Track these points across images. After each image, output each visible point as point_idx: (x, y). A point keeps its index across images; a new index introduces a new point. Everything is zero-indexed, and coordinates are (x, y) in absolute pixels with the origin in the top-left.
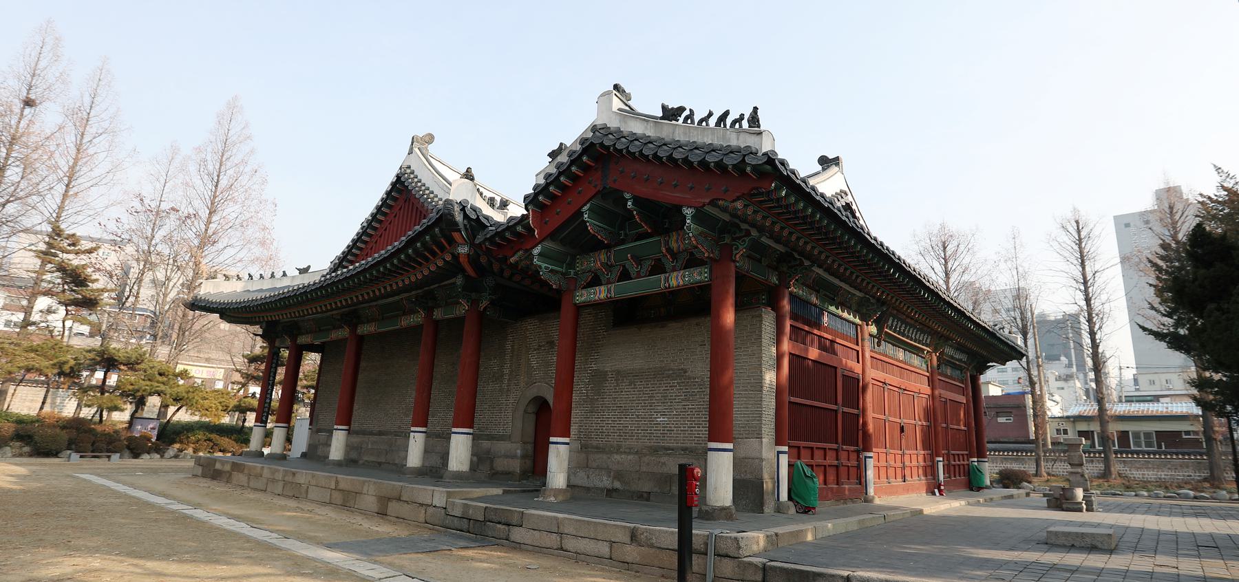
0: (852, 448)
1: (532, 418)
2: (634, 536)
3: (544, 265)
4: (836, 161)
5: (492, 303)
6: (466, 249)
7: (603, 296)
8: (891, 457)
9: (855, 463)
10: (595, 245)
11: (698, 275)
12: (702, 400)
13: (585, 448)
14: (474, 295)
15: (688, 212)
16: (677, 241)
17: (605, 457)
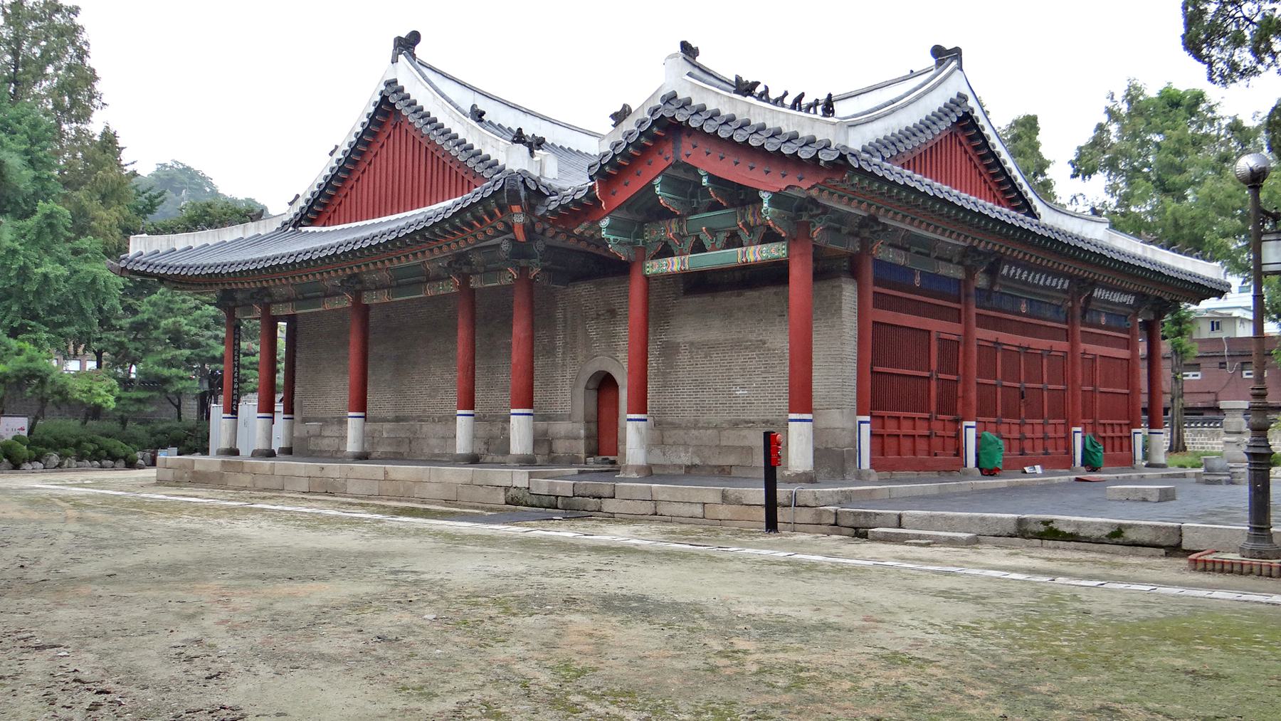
0: (951, 417)
1: (594, 394)
2: (725, 498)
3: (612, 238)
4: (956, 53)
5: (544, 269)
6: (522, 218)
7: (676, 268)
8: (1050, 429)
9: (953, 434)
10: (665, 214)
11: (774, 251)
12: (782, 371)
13: (658, 424)
14: (523, 263)
15: (765, 196)
16: (753, 214)
17: (682, 432)
